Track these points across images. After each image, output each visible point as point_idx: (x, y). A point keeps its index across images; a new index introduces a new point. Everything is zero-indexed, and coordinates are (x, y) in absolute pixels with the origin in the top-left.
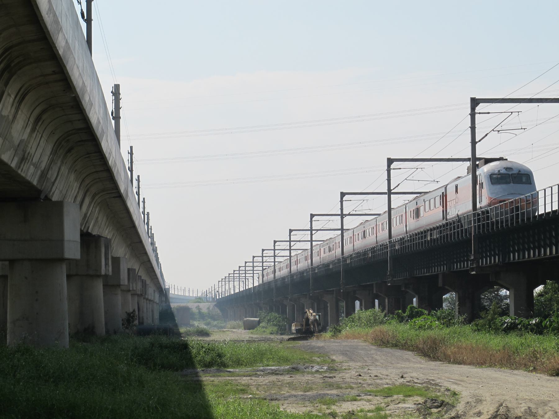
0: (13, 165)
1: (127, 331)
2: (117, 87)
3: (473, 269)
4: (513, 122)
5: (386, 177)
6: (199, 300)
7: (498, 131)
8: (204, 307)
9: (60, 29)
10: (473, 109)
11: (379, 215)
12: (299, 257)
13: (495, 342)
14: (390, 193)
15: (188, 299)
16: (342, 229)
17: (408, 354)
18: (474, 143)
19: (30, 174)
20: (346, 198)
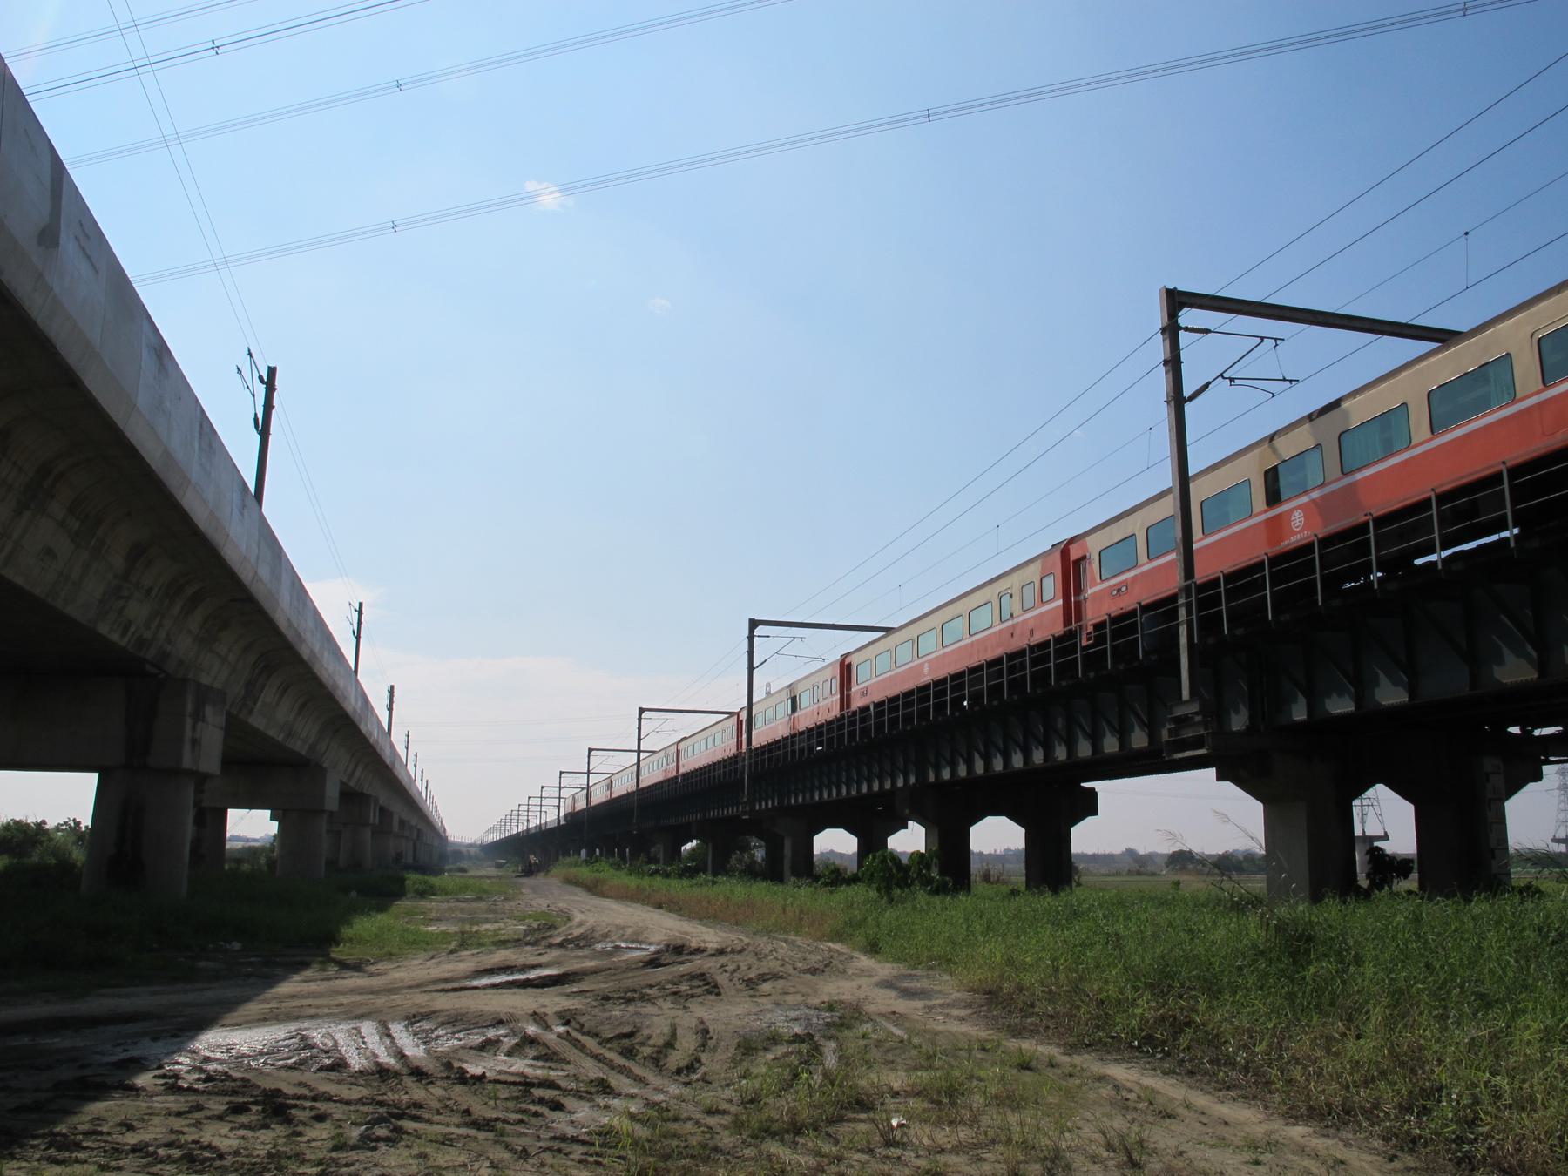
0: (280, 738)
1: (1445, 1079)
2: (272, 372)
3: (745, 813)
4: (1264, 362)
5: (746, 648)
6: (470, 845)
7: (1232, 380)
8: (472, 850)
9: (302, 640)
10: (1173, 315)
11: (888, 631)
12: (617, 776)
13: (632, 882)
14: (589, 772)
15: (460, 845)
16: (639, 751)
17: (579, 890)
18: (639, 739)
19: (299, 746)
20: (759, 630)
